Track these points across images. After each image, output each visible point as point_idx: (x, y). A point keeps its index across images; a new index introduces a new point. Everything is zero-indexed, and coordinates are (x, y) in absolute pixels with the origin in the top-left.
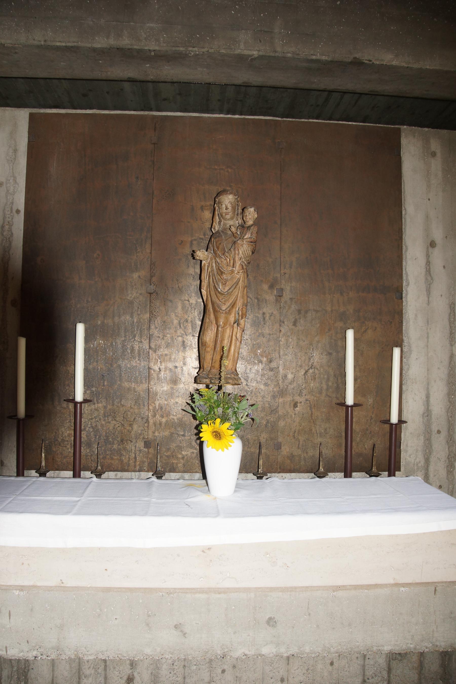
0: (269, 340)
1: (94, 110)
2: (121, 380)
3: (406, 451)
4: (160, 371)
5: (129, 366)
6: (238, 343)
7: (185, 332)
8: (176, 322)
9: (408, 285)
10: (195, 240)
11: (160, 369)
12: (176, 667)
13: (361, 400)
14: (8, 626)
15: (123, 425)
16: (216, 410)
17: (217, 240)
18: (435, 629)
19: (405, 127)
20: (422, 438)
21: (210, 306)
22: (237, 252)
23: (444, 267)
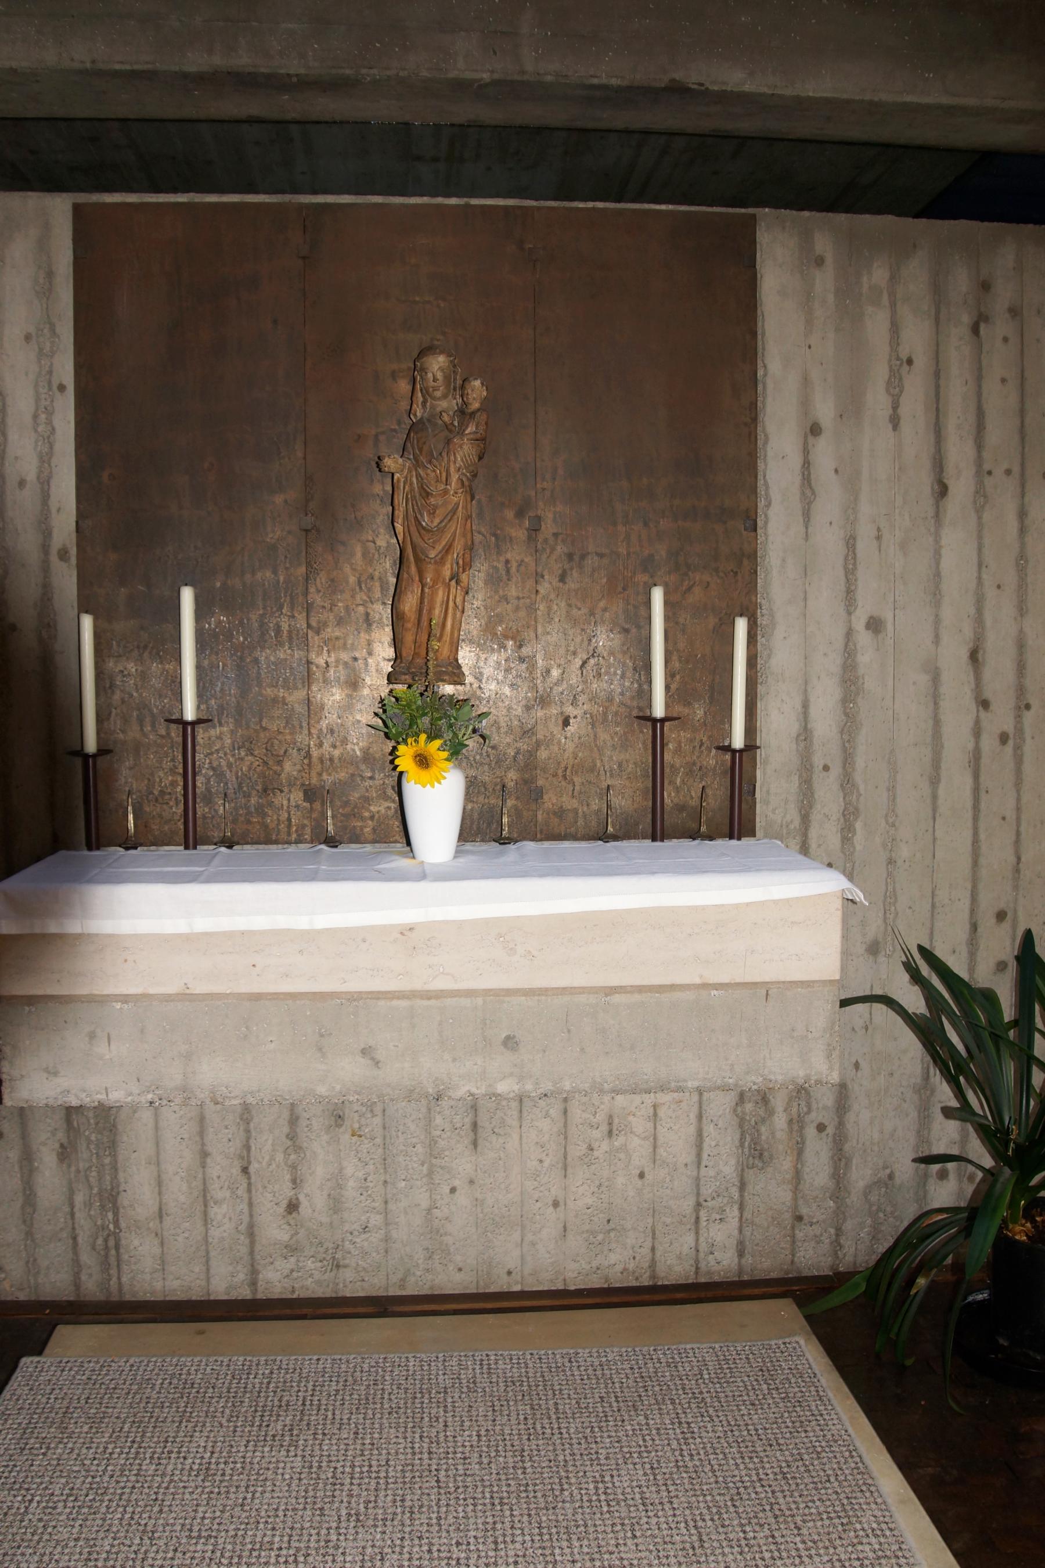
0: (517, 609)
1: (192, 194)
2: (260, 685)
3: (767, 803)
4: (328, 666)
5: (272, 659)
6: (458, 614)
7: (369, 597)
8: (352, 580)
9: (769, 505)
10: (383, 433)
11: (327, 663)
12: (371, 1185)
13: (678, 710)
14: (108, 1057)
15: (265, 763)
16: (419, 721)
17: (419, 435)
18: (768, 1056)
19: (767, 210)
20: (795, 779)
21: (409, 550)
22: (452, 458)
23: (836, 471)
